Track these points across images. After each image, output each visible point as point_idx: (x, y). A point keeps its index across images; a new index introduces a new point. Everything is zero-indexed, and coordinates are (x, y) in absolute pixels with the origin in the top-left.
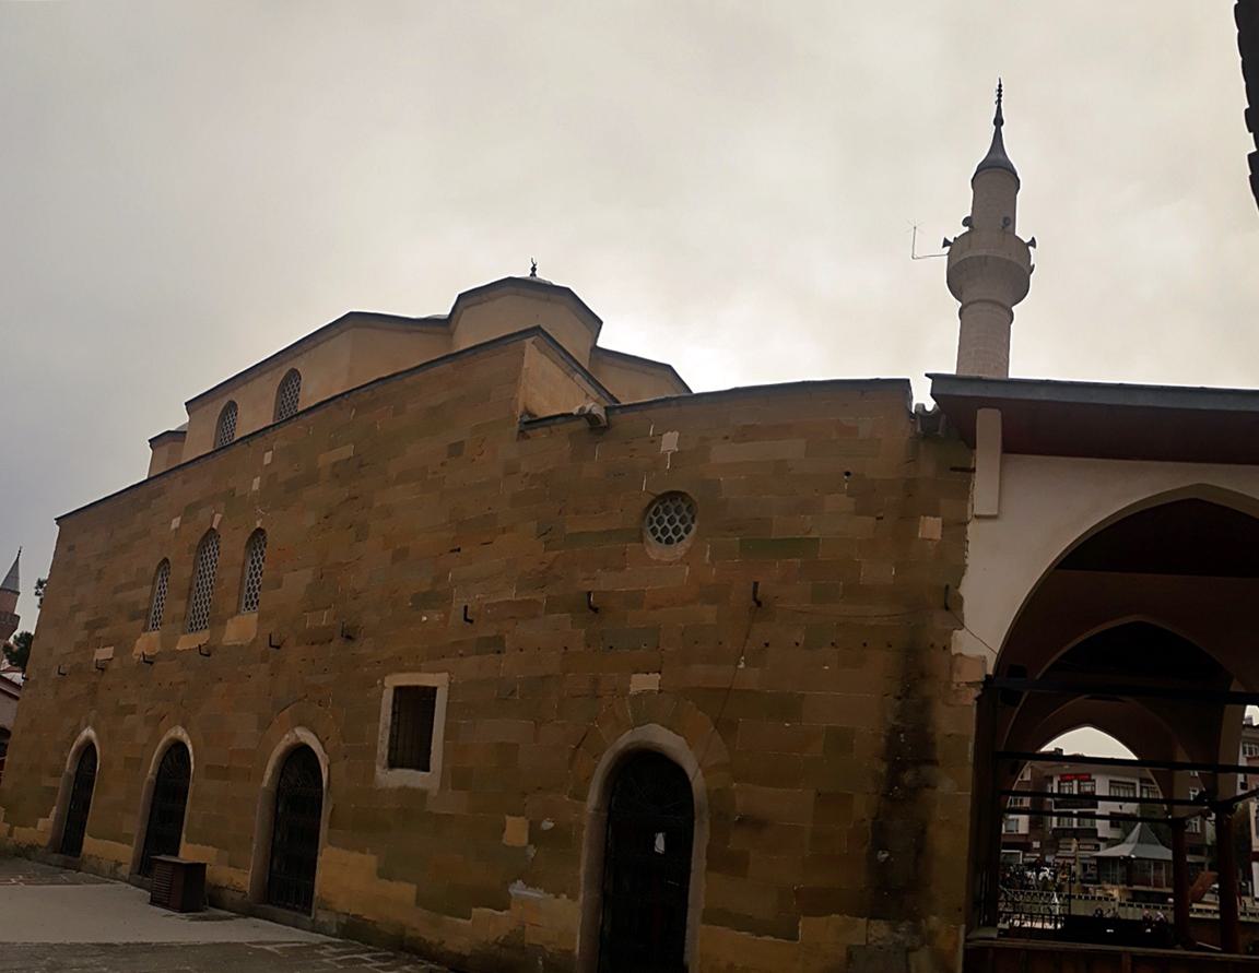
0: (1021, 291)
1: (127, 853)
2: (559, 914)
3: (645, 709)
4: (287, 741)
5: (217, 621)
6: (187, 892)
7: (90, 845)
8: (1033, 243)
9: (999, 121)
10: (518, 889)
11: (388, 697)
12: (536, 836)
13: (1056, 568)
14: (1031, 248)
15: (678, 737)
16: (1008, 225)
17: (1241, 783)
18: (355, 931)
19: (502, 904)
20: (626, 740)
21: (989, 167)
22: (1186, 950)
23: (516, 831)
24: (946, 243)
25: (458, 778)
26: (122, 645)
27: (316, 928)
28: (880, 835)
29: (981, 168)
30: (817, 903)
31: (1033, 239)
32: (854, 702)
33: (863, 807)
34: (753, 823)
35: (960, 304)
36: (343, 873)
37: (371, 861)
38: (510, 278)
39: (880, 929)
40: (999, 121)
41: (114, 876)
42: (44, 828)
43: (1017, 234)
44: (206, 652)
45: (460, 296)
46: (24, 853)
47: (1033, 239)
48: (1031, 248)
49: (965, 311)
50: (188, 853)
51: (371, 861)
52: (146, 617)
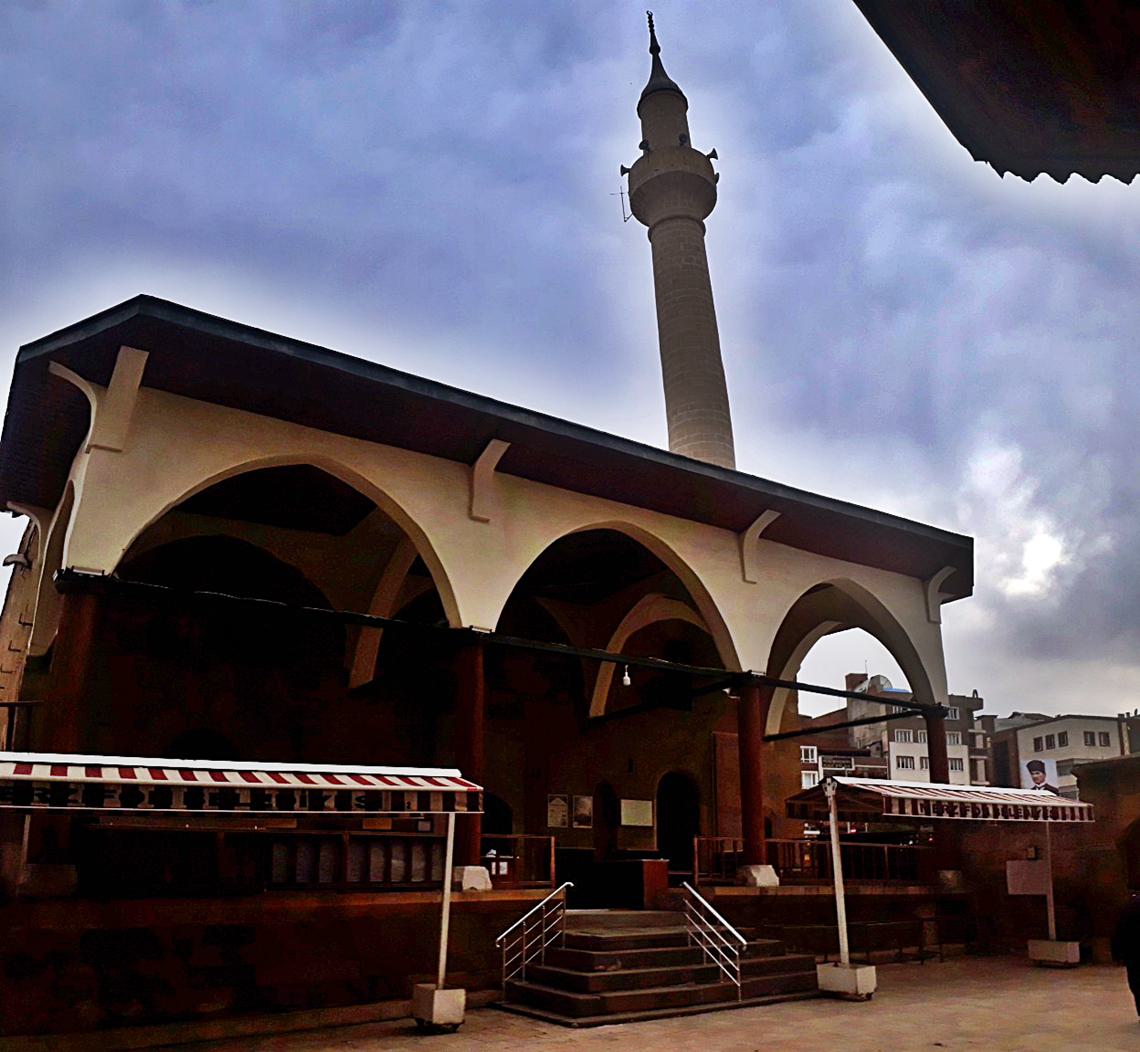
0: (710, 203)
8: (714, 154)
9: (655, 49)
13: (419, 558)
14: (712, 160)
15: (775, 875)
16: (685, 142)
17: (87, 775)
21: (654, 91)
22: (550, 900)
24: (624, 170)
29: (645, 95)
31: (714, 151)
35: (647, 228)
38: (638, 109)
40: (655, 49)
43: (693, 147)
45: (142, 296)
47: (714, 151)
48: (712, 160)
49: (654, 233)
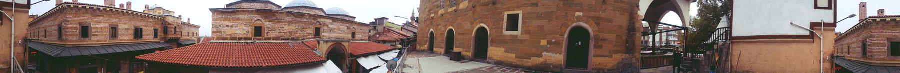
1: (443, 50)
2: (558, 58)
3: (579, 19)
4: (478, 26)
5: (457, 5)
6: (458, 58)
7: (435, 49)
10: (545, 53)
11: (506, 17)
12: (549, 43)
18: (499, 63)
19: (541, 56)
20: (574, 25)
23: (544, 42)
25: (526, 32)
26: (436, 13)
27: (488, 63)
28: (627, 42)
30: (617, 52)
32: (621, 21)
33: (624, 38)
34: (604, 40)
36: (495, 52)
37: (503, 49)
39: (627, 56)
41: (441, 54)
42: (426, 47)
44: (455, 11)
46: (423, 51)
50: (456, 50)
51: (503, 49)
52: (440, 7)
